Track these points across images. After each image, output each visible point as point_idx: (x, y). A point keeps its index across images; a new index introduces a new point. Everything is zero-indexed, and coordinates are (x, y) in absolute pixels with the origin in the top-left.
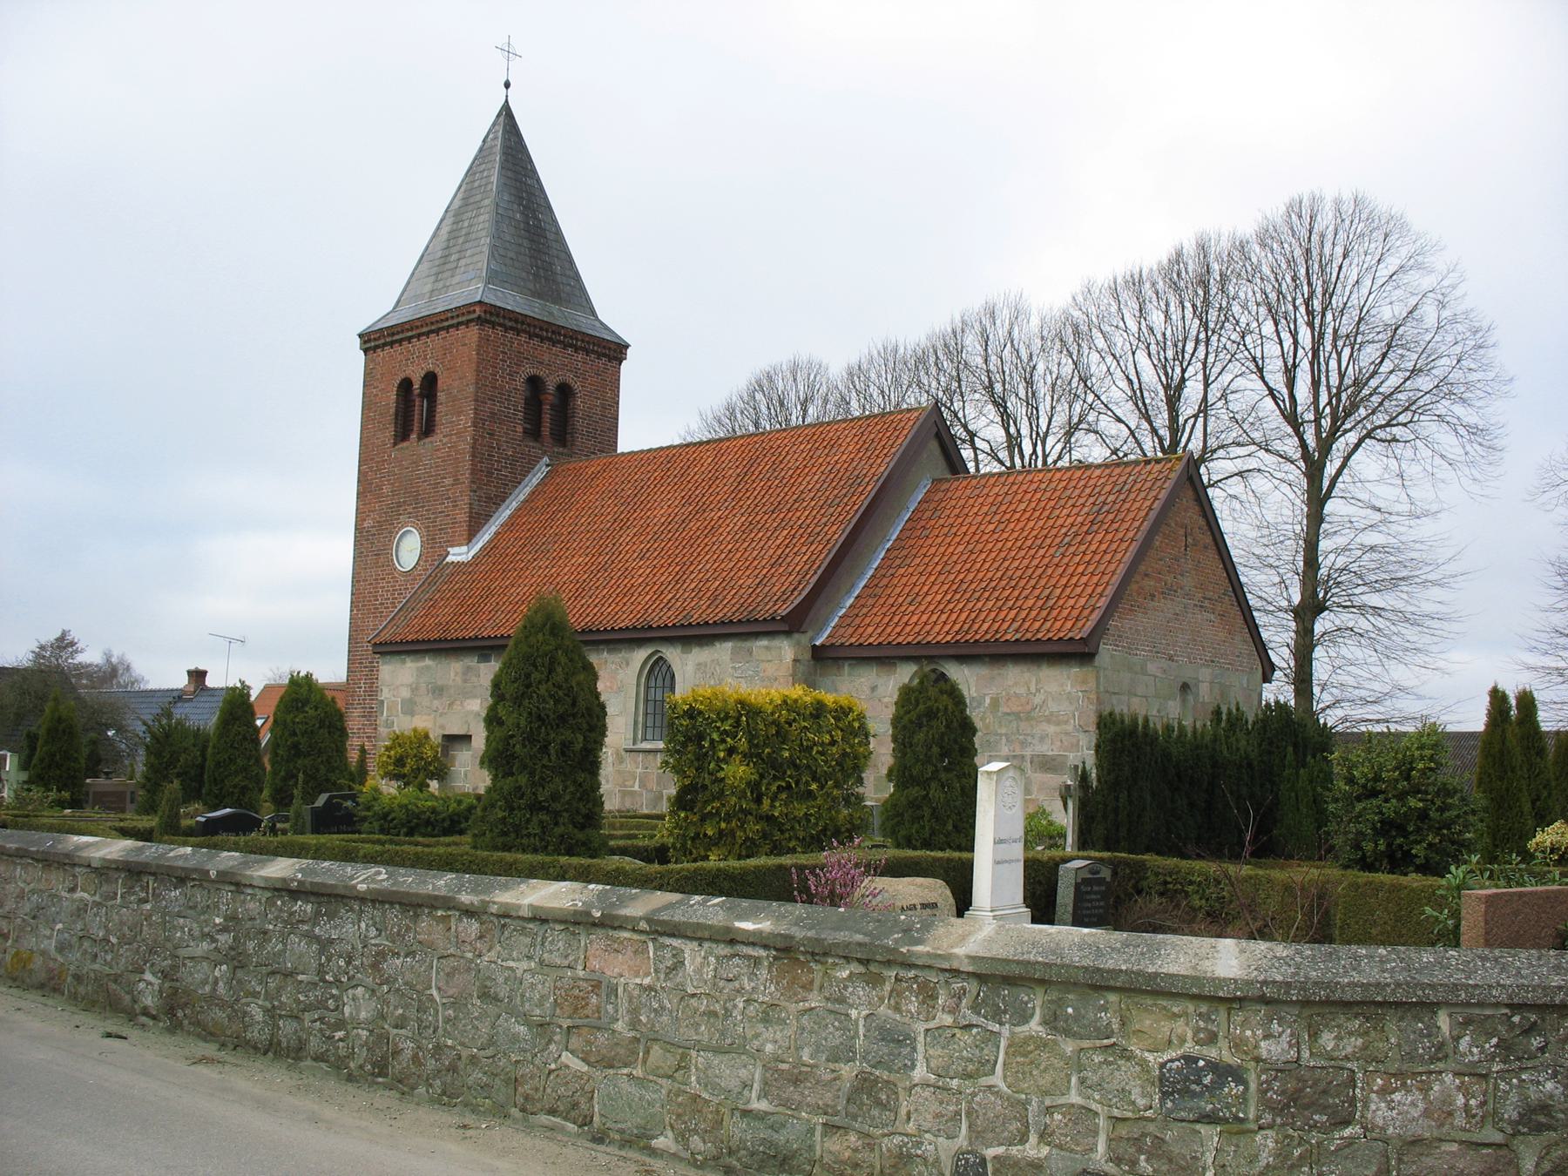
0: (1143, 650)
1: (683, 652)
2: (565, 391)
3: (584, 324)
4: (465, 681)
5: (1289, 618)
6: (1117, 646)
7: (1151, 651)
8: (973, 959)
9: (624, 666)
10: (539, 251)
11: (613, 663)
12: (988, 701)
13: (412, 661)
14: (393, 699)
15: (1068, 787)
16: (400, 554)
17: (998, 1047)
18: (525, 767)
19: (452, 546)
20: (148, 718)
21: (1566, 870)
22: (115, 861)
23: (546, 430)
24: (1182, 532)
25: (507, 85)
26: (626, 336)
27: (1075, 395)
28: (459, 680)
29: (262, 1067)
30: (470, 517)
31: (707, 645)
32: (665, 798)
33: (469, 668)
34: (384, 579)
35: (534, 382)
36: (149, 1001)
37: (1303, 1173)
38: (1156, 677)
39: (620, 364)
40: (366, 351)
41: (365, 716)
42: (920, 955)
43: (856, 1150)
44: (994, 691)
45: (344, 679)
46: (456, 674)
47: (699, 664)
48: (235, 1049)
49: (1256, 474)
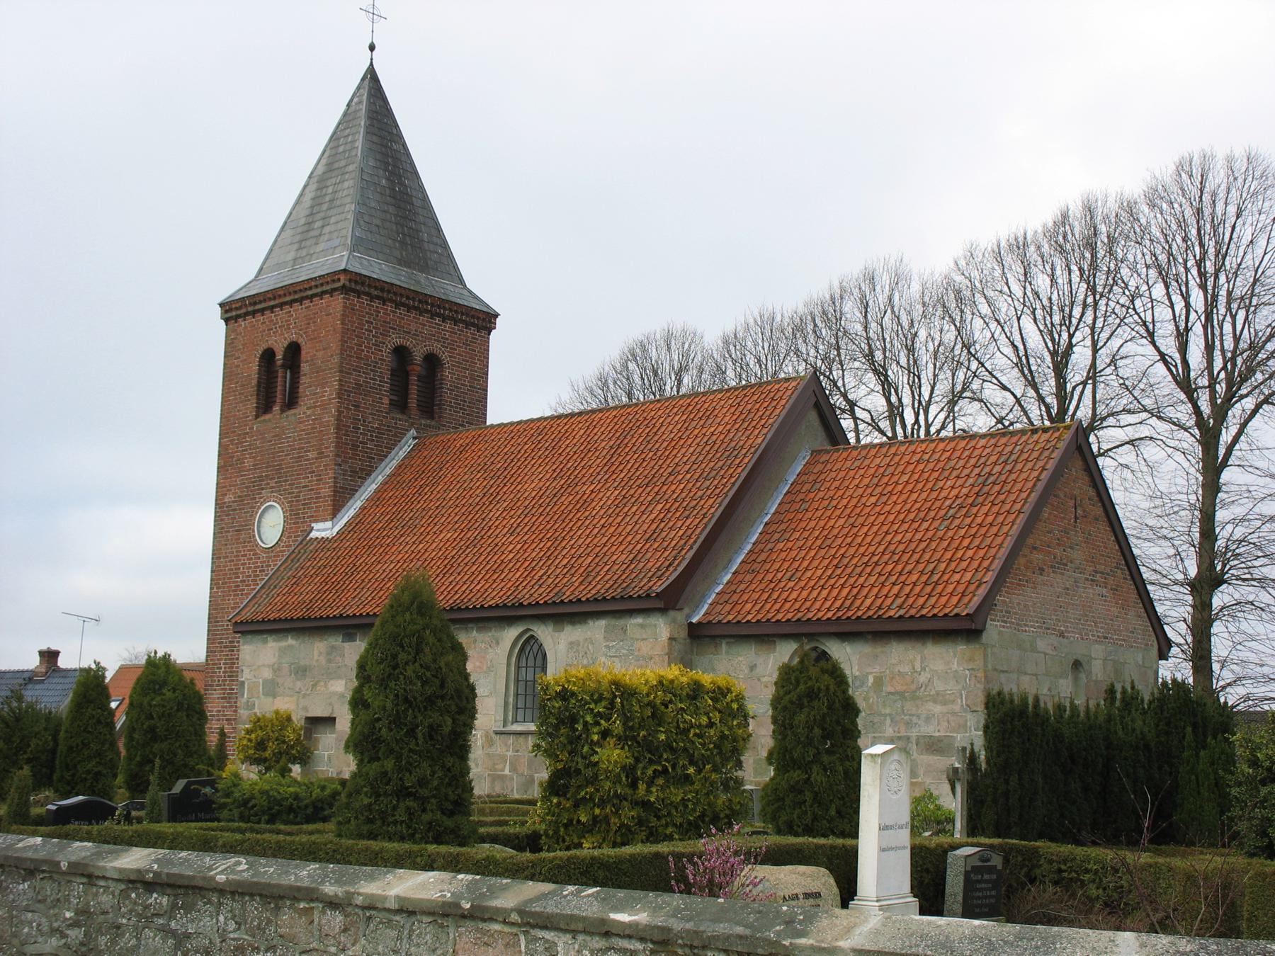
0: (1032, 626)
1: (554, 631)
2: (432, 361)
3: (453, 295)
4: (329, 661)
6: (1006, 622)
7: (1041, 627)
12: (871, 679)
13: (274, 640)
15: (956, 770)
18: (392, 751)
19: (316, 521)
24: (1071, 503)
25: (372, 48)
26: (495, 305)
28: (323, 660)
31: (580, 623)
35: (401, 353)
38: (1045, 654)
40: (227, 321)
44: (877, 669)
46: (320, 653)
47: (571, 643)
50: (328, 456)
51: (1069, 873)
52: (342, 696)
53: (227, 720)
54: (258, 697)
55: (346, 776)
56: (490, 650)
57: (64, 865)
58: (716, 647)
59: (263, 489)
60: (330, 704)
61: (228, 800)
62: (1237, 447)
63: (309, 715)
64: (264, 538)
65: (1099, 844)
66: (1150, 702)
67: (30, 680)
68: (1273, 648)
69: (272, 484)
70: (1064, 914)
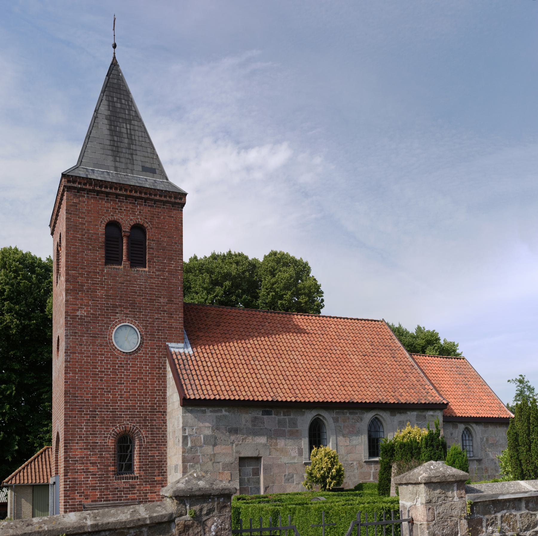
1: (391, 415)
4: (254, 425)
5: (457, 432)
10: (117, 147)
11: (353, 419)
12: (485, 439)
13: (211, 412)
16: (124, 328)
20: (512, 404)
22: (21, 510)
25: (115, 46)
26: (183, 187)
29: (251, 412)
31: (403, 413)
35: (113, 225)
43: (80, 516)
44: (486, 435)
46: (247, 421)
47: (400, 421)
48: (431, 501)
49: (410, 513)
50: (178, 304)
51: (269, 295)
55: (297, 259)
58: (195, 257)
59: (117, 313)
62: (238, 474)
66: (227, 255)
67: (191, 448)
68: (350, 534)
70: (389, 330)
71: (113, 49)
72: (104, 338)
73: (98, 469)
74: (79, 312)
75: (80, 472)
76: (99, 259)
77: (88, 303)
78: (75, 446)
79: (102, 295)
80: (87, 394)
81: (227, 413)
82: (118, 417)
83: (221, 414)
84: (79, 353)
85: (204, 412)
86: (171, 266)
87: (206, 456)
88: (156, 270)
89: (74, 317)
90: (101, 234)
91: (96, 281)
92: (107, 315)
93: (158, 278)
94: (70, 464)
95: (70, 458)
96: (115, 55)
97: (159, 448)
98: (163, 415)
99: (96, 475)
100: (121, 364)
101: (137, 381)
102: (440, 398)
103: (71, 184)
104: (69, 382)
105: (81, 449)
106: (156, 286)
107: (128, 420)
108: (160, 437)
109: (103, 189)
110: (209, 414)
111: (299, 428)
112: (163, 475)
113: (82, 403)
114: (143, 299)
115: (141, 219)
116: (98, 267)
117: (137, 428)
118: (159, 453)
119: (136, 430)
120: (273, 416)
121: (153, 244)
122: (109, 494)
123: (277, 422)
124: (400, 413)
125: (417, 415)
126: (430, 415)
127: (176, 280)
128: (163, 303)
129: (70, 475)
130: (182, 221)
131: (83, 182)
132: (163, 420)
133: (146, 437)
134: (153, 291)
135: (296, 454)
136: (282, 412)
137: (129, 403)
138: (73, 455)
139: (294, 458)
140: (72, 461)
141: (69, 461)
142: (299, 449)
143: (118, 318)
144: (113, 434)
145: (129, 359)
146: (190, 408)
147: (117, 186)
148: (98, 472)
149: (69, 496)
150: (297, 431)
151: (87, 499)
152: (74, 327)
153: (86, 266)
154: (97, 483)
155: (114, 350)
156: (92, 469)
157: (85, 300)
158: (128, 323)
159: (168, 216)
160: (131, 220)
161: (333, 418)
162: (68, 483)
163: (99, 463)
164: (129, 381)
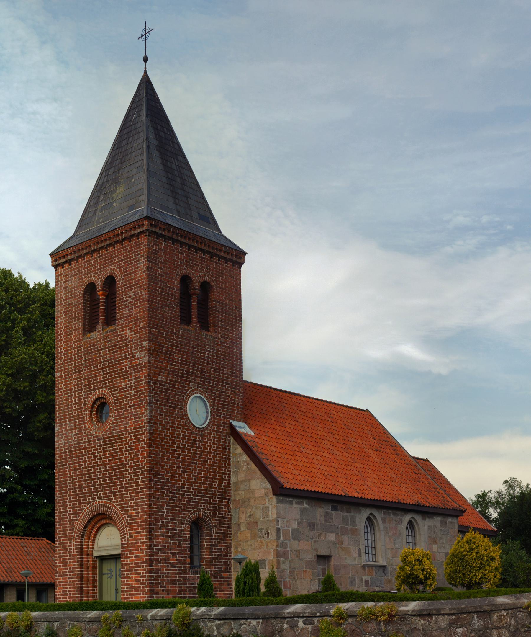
2: (205, 287)
3: (202, 230)
4: (326, 521)
8: (413, 611)
9: (400, 523)
13: (297, 503)
14: (286, 528)
15: (491, 516)
17: (138, 211)
18: (455, 564)
21: (525, 601)
23: (194, 319)
25: (146, 59)
27: (367, 533)
28: (323, 519)
29: (323, 506)
30: (84, 300)
32: (277, 505)
33: (327, 513)
34: (180, 428)
35: (185, 280)
36: (500, 571)
37: (371, 633)
39: (240, 268)
40: (56, 267)
41: (169, 536)
42: (200, 547)
45: (244, 379)
47: (429, 526)
52: (303, 511)
53: (171, 553)
54: (289, 540)
56: (399, 526)
57: (149, 618)
60: (329, 548)
61: (299, 632)
63: (319, 553)
64: (198, 400)
65: (315, 592)
69: (198, 380)
71: (144, 63)
72: (180, 409)
73: (177, 560)
74: (160, 376)
75: (163, 563)
76: (176, 318)
77: (167, 367)
78: (158, 532)
79: (178, 359)
80: (168, 473)
81: (308, 506)
82: (193, 502)
83: (303, 507)
84: (160, 425)
85: (291, 503)
86: (233, 334)
87: (293, 551)
88: (221, 336)
89: (156, 382)
90: (177, 290)
91: (173, 342)
92: (183, 383)
93: (223, 346)
94: (154, 552)
95: (155, 546)
96: (145, 70)
97: (225, 540)
98: (228, 502)
99: (175, 567)
100: (194, 440)
101: (207, 462)
102: (455, 504)
103: (153, 229)
104: (153, 457)
105: (163, 536)
106: (222, 355)
107: (201, 506)
108: (226, 528)
109: (179, 238)
110: (295, 506)
111: (358, 527)
112: (229, 572)
113: (163, 482)
114: (212, 368)
115: (208, 276)
116: (174, 327)
117: (208, 515)
118: (226, 546)
119: (207, 518)
120: (339, 512)
121: (218, 306)
122: (186, 590)
123: (342, 519)
124: (429, 517)
125: (441, 520)
126: (449, 522)
127: (237, 350)
128: (227, 374)
129: (155, 566)
130: (240, 283)
131: (163, 227)
132: (228, 509)
133: (216, 526)
134: (219, 360)
135: (357, 556)
136: (345, 508)
137: (201, 487)
138: (157, 542)
139: (355, 558)
140: (156, 549)
141: (153, 549)
142: (358, 550)
143: (192, 388)
144: (189, 521)
145: (201, 435)
146: (282, 498)
147: (191, 237)
148: (177, 563)
149: (153, 590)
150: (356, 529)
151: (168, 594)
152: (156, 394)
153: (164, 324)
154: (176, 577)
155: (189, 424)
156: (172, 560)
157: (165, 363)
158: (200, 394)
159: (230, 276)
160: (200, 276)
161: (382, 518)
162: (153, 574)
163: (178, 553)
164: (201, 461)
